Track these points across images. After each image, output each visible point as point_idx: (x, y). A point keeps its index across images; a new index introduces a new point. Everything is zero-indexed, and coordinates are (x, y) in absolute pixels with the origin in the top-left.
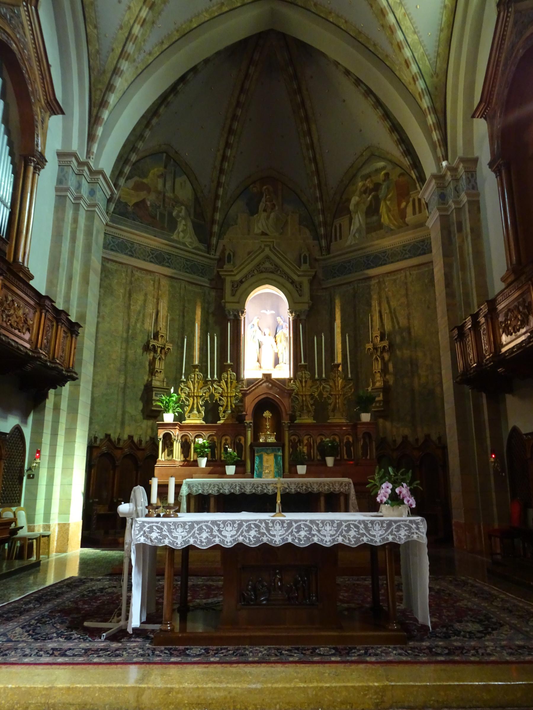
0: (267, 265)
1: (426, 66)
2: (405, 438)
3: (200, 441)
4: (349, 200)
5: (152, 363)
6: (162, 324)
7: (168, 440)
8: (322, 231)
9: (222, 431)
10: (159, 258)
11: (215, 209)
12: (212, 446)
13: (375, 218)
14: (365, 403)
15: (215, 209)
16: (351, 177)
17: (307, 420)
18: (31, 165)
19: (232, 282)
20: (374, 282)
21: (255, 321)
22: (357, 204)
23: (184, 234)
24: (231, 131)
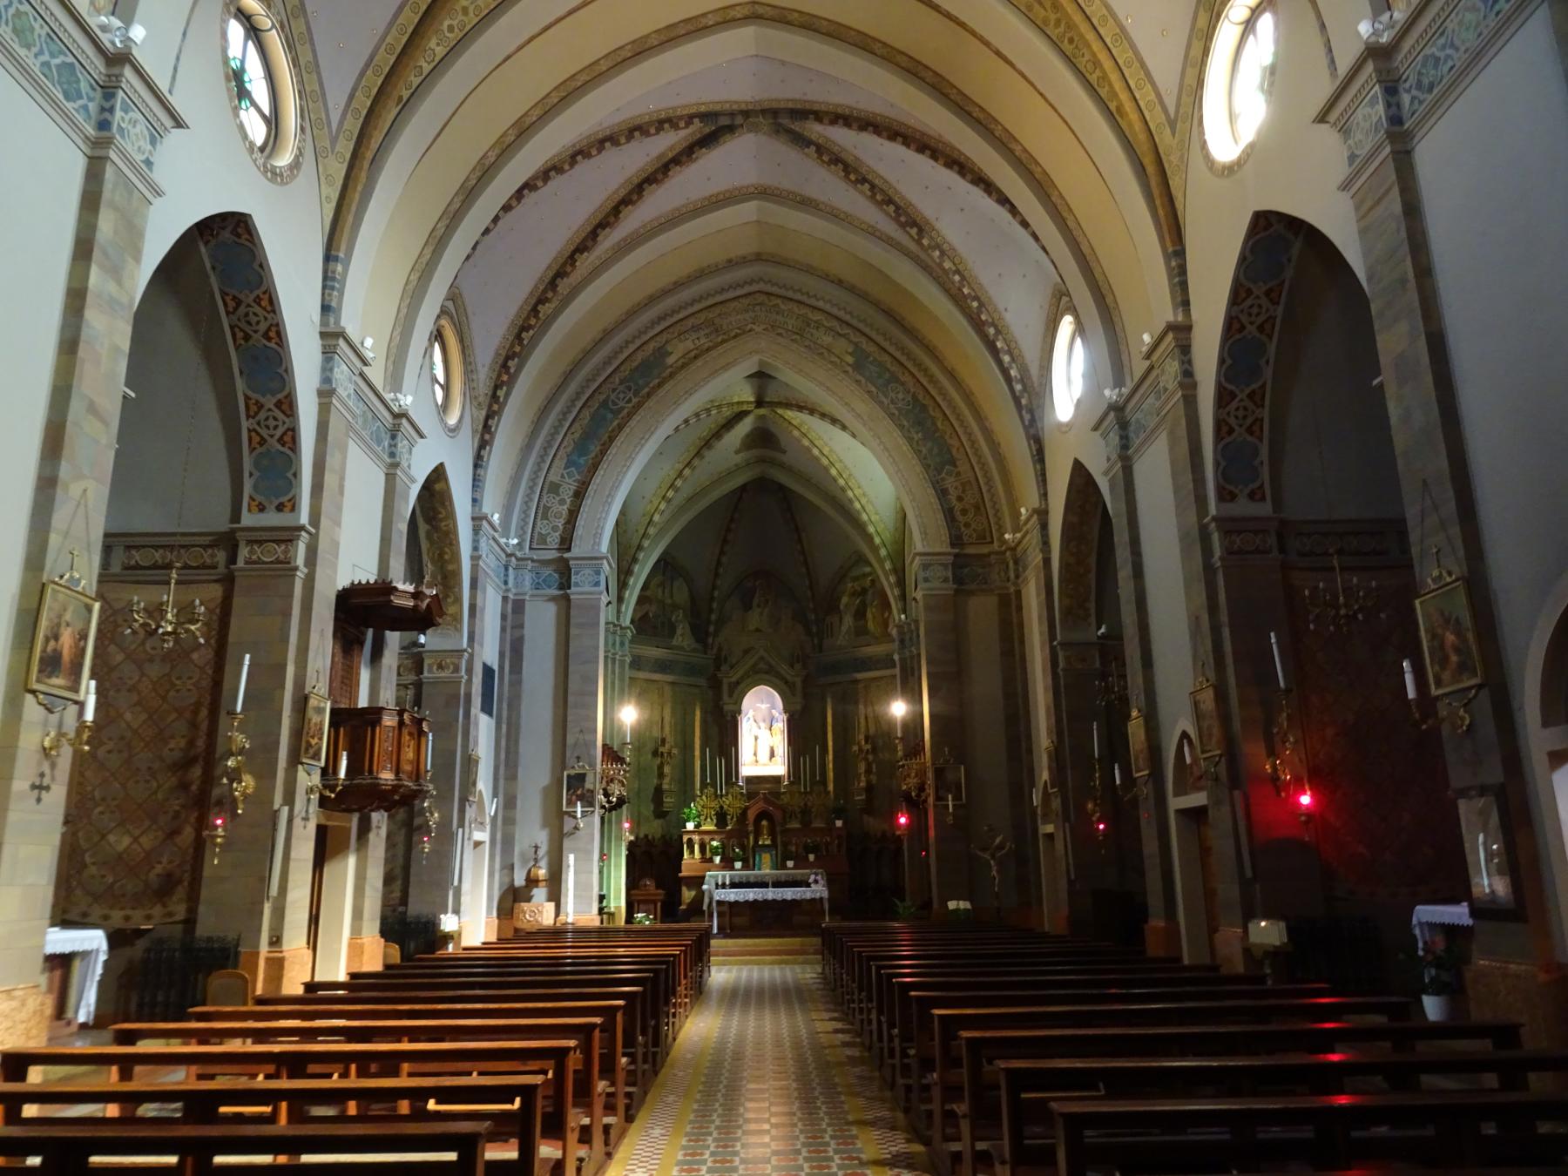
0: (762, 665)
1: (887, 536)
3: (715, 843)
4: (839, 599)
5: (661, 767)
6: (667, 729)
7: (690, 843)
8: (814, 629)
9: (730, 835)
10: (662, 666)
11: (711, 611)
12: (724, 846)
14: (839, 812)
15: (711, 611)
17: (795, 825)
20: (860, 686)
21: (751, 713)
23: (683, 637)
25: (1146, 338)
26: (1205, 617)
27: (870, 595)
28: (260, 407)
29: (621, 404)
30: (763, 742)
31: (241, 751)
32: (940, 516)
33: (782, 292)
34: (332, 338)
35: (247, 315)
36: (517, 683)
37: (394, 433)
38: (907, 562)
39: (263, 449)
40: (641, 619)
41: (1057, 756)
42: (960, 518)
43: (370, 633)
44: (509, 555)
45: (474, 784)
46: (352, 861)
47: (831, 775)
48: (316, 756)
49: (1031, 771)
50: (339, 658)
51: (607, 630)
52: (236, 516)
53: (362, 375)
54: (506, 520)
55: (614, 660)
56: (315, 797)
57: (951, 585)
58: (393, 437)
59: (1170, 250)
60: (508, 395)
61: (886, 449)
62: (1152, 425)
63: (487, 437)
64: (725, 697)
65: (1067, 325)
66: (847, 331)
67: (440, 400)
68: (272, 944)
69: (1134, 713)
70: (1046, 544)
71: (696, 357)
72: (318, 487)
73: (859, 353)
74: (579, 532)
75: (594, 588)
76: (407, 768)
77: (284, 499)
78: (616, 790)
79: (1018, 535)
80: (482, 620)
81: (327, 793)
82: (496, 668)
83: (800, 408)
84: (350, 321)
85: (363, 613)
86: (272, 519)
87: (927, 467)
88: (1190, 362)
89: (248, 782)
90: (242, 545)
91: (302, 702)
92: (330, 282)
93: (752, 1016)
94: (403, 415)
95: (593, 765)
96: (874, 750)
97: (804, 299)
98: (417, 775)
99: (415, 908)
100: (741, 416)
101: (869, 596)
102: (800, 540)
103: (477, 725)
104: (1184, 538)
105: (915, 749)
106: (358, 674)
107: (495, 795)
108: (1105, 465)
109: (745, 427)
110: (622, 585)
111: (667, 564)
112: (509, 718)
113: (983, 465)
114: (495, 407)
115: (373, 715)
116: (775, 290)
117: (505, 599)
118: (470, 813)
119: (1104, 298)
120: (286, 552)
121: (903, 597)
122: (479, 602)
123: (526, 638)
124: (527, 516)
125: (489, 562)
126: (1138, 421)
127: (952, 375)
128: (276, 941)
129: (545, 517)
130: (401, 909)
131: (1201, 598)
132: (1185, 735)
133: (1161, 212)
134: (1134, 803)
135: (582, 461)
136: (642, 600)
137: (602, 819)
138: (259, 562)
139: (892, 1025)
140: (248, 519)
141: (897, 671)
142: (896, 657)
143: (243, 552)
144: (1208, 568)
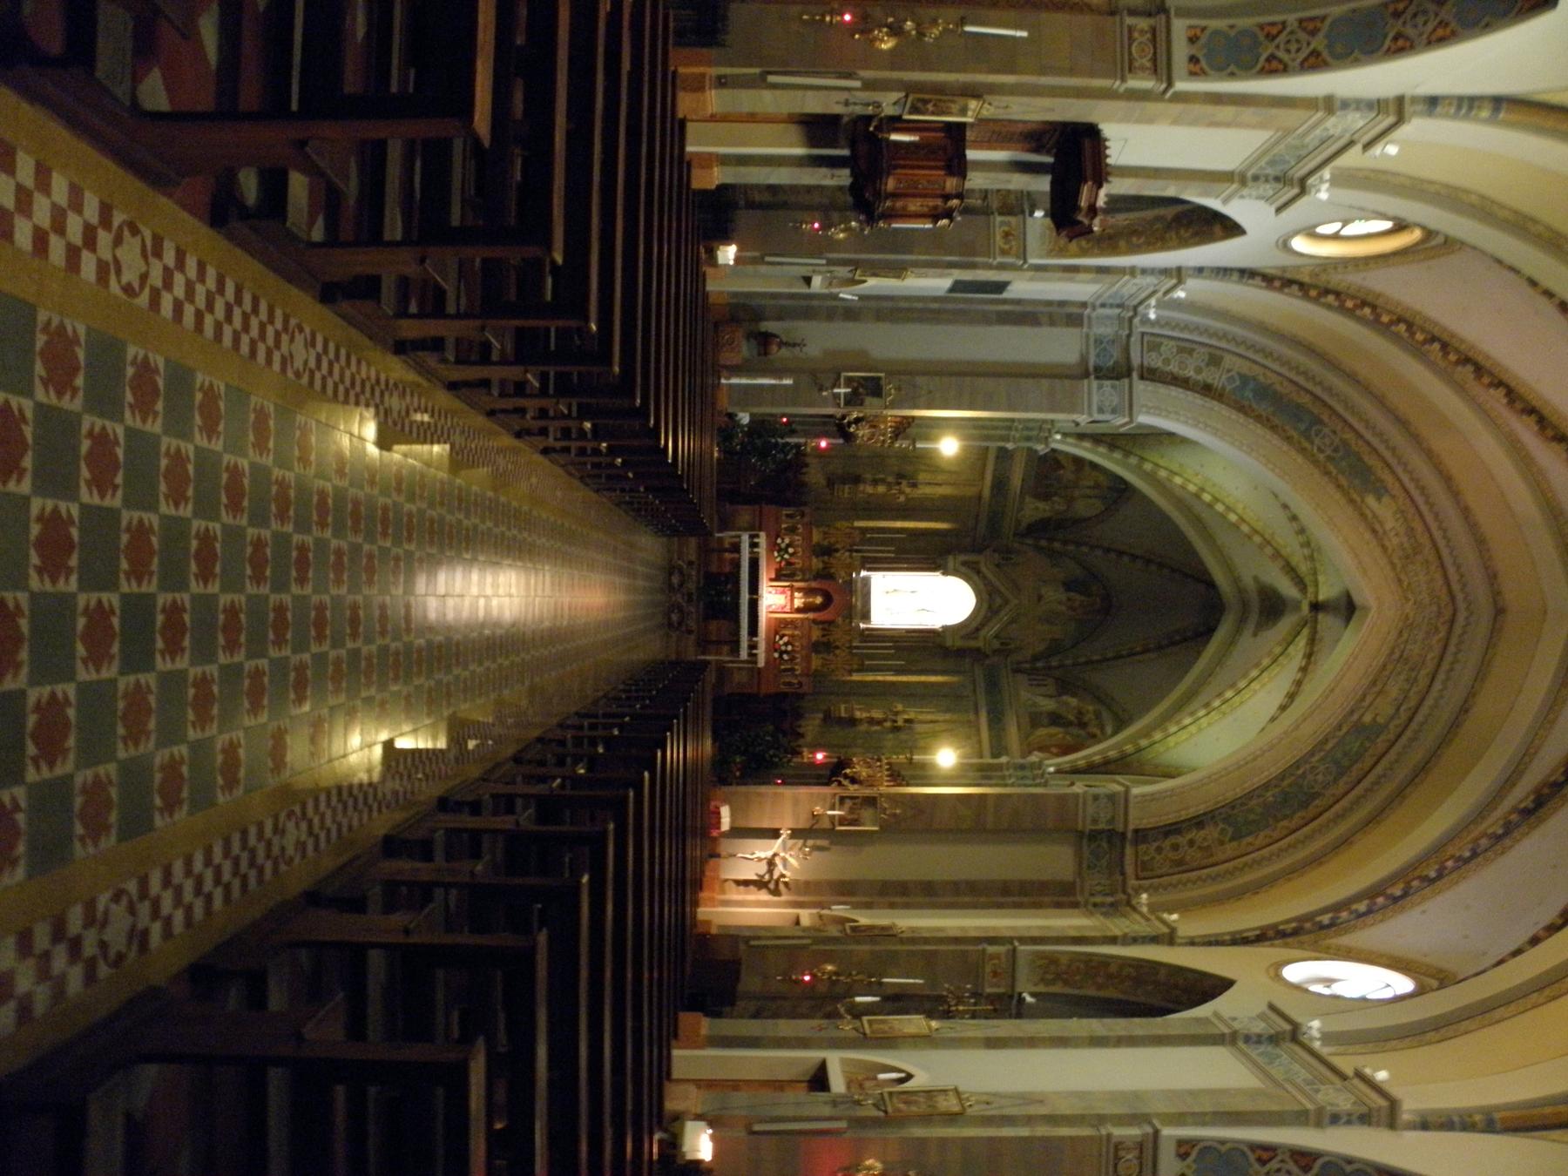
2: (802, 736)
4: (1074, 695)
8: (1039, 664)
10: (1000, 485)
13: (1046, 721)
15: (1065, 543)
16: (1100, 698)
18: (435, 738)
19: (977, 563)
20: (972, 717)
22: (1067, 704)
23: (1035, 509)
24: (1148, 562)
25: (1382, 1075)
26: (1043, 1111)
27: (1077, 731)
28: (1313, 33)
29: (1317, 441)
30: (919, 600)
31: (921, 34)
32: (1172, 818)
33: (1454, 640)
34: (1398, 109)
35: (1425, 12)
36: (986, 319)
37: (1281, 179)
38: (1118, 778)
39: (1261, 38)
40: (1057, 462)
41: (886, 934)
42: (1167, 843)
43: (1049, 159)
44: (1135, 308)
45: (875, 275)
46: (800, 151)
47: (870, 677)
48: (914, 110)
49: (869, 906)
50: (1020, 127)
51: (1044, 421)
52: (1185, 13)
53: (1351, 143)
54: (1178, 305)
55: (1010, 428)
56: (870, 110)
57: (1090, 827)
58: (1277, 179)
59: (1497, 1116)
60: (1329, 307)
61: (1255, 759)
62: (1273, 1072)
63: (1277, 284)
64: (962, 558)
65: (1402, 984)
66: (1404, 716)
67: (1321, 230)
68: (719, 78)
69: (934, 1024)
70: (1135, 940)
71: (1374, 531)
72: (1217, 99)
73: (1376, 729)
74: (1162, 390)
75: (1097, 406)
76: (899, 204)
77: (1203, 63)
78: (863, 432)
79: (1145, 909)
80: (1060, 279)
81: (874, 123)
82: (1005, 295)
83: (1309, 656)
84: (1417, 127)
85: (1073, 154)
86: (1181, 51)
87: (1232, 805)
88: (1349, 1122)
89: (887, 45)
90: (1151, 21)
91: (975, 92)
92: (1466, 105)
93: (475, 576)
94: (1303, 190)
95: (893, 405)
96: (896, 729)
97: (1445, 666)
98: (891, 215)
99: (743, 218)
100: (1300, 582)
101: (1075, 731)
102: (1146, 651)
103: (941, 276)
104: (1136, 1096)
105: (897, 777)
106: (1002, 149)
107: (862, 298)
108: (1226, 1014)
109: (1287, 588)
110: (1097, 439)
111: (1124, 490)
112: (946, 311)
113: (1231, 873)
114: (1313, 293)
115: (958, 166)
116: (1458, 630)
117: (1084, 305)
118: (843, 271)
119: (1436, 1029)
120: (1143, 68)
121: (1076, 771)
122: (1082, 276)
123: (1036, 330)
124: (1182, 330)
125: (1128, 287)
126: (1279, 1057)
127: (1345, 842)
128: (722, 82)
129: (1181, 350)
130: (742, 203)
131: (1064, 1108)
132: (909, 1077)
133: (1548, 1110)
134: (833, 1015)
135: (1249, 394)
136: (1079, 462)
137: (831, 416)
138: (1131, 40)
139: (621, 727)
140: (1180, 27)
141: (989, 760)
142: (1004, 759)
143: (1143, 23)
144: (1101, 1119)
